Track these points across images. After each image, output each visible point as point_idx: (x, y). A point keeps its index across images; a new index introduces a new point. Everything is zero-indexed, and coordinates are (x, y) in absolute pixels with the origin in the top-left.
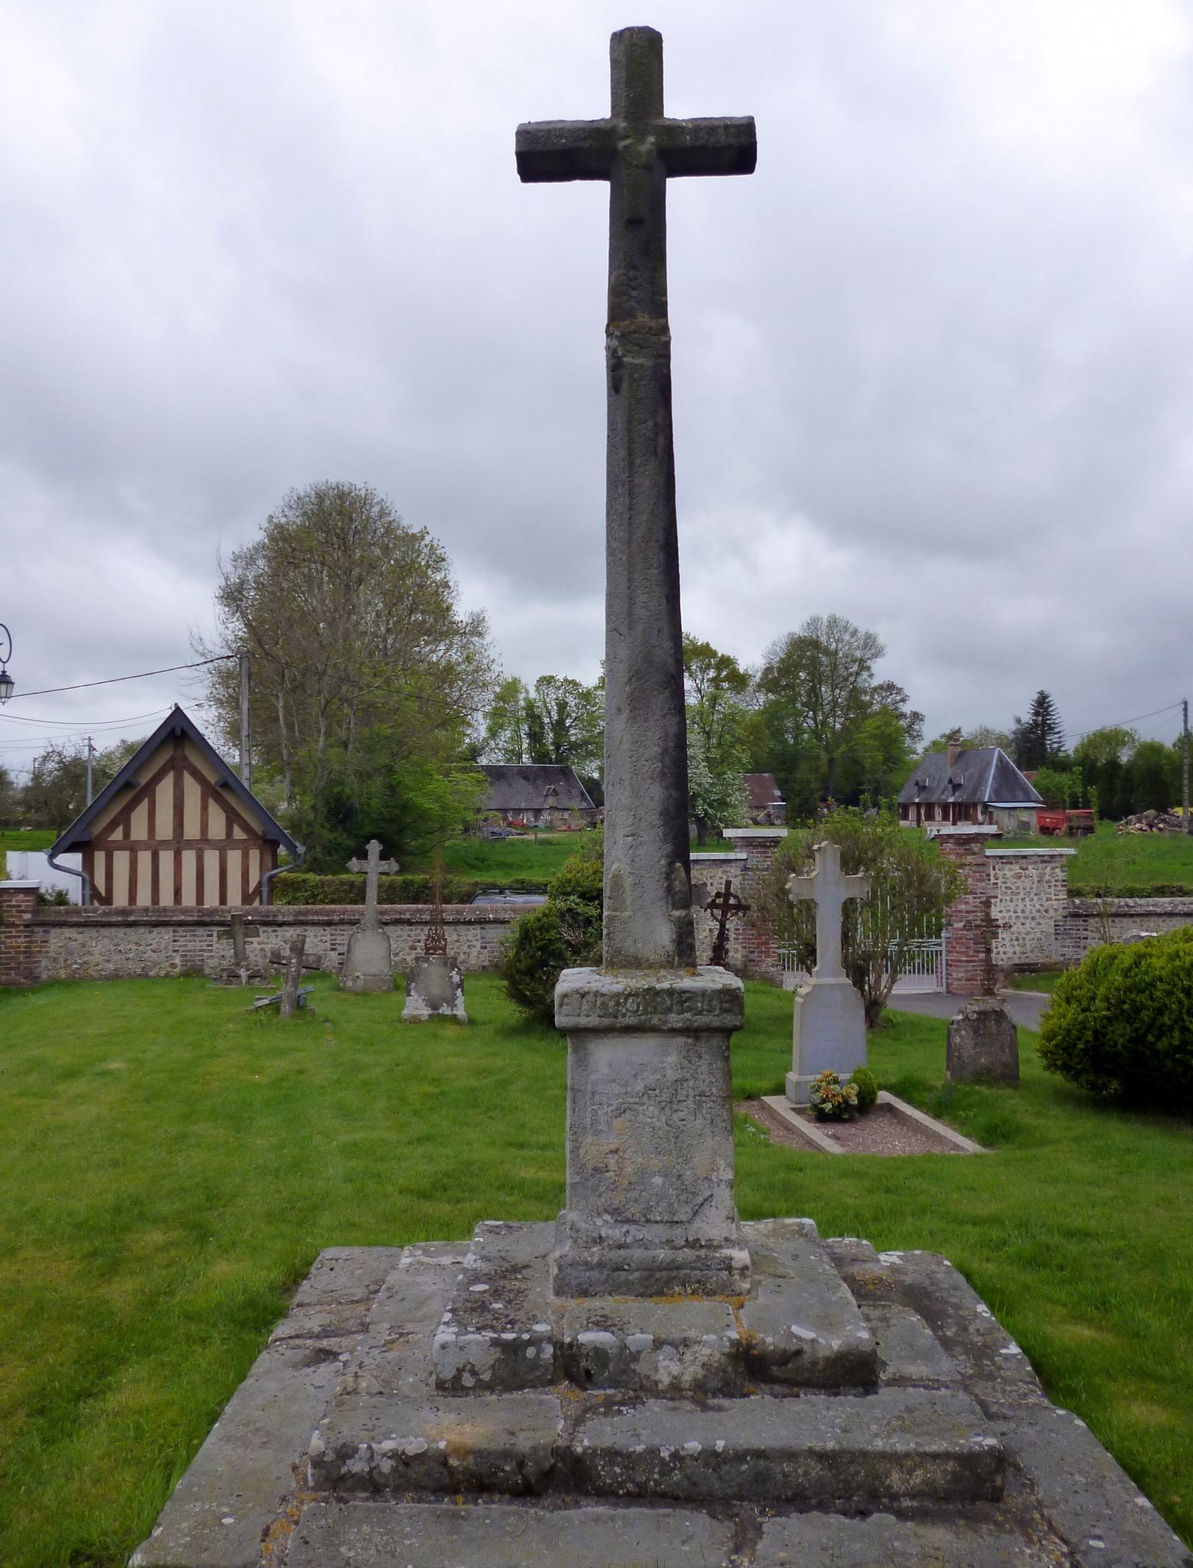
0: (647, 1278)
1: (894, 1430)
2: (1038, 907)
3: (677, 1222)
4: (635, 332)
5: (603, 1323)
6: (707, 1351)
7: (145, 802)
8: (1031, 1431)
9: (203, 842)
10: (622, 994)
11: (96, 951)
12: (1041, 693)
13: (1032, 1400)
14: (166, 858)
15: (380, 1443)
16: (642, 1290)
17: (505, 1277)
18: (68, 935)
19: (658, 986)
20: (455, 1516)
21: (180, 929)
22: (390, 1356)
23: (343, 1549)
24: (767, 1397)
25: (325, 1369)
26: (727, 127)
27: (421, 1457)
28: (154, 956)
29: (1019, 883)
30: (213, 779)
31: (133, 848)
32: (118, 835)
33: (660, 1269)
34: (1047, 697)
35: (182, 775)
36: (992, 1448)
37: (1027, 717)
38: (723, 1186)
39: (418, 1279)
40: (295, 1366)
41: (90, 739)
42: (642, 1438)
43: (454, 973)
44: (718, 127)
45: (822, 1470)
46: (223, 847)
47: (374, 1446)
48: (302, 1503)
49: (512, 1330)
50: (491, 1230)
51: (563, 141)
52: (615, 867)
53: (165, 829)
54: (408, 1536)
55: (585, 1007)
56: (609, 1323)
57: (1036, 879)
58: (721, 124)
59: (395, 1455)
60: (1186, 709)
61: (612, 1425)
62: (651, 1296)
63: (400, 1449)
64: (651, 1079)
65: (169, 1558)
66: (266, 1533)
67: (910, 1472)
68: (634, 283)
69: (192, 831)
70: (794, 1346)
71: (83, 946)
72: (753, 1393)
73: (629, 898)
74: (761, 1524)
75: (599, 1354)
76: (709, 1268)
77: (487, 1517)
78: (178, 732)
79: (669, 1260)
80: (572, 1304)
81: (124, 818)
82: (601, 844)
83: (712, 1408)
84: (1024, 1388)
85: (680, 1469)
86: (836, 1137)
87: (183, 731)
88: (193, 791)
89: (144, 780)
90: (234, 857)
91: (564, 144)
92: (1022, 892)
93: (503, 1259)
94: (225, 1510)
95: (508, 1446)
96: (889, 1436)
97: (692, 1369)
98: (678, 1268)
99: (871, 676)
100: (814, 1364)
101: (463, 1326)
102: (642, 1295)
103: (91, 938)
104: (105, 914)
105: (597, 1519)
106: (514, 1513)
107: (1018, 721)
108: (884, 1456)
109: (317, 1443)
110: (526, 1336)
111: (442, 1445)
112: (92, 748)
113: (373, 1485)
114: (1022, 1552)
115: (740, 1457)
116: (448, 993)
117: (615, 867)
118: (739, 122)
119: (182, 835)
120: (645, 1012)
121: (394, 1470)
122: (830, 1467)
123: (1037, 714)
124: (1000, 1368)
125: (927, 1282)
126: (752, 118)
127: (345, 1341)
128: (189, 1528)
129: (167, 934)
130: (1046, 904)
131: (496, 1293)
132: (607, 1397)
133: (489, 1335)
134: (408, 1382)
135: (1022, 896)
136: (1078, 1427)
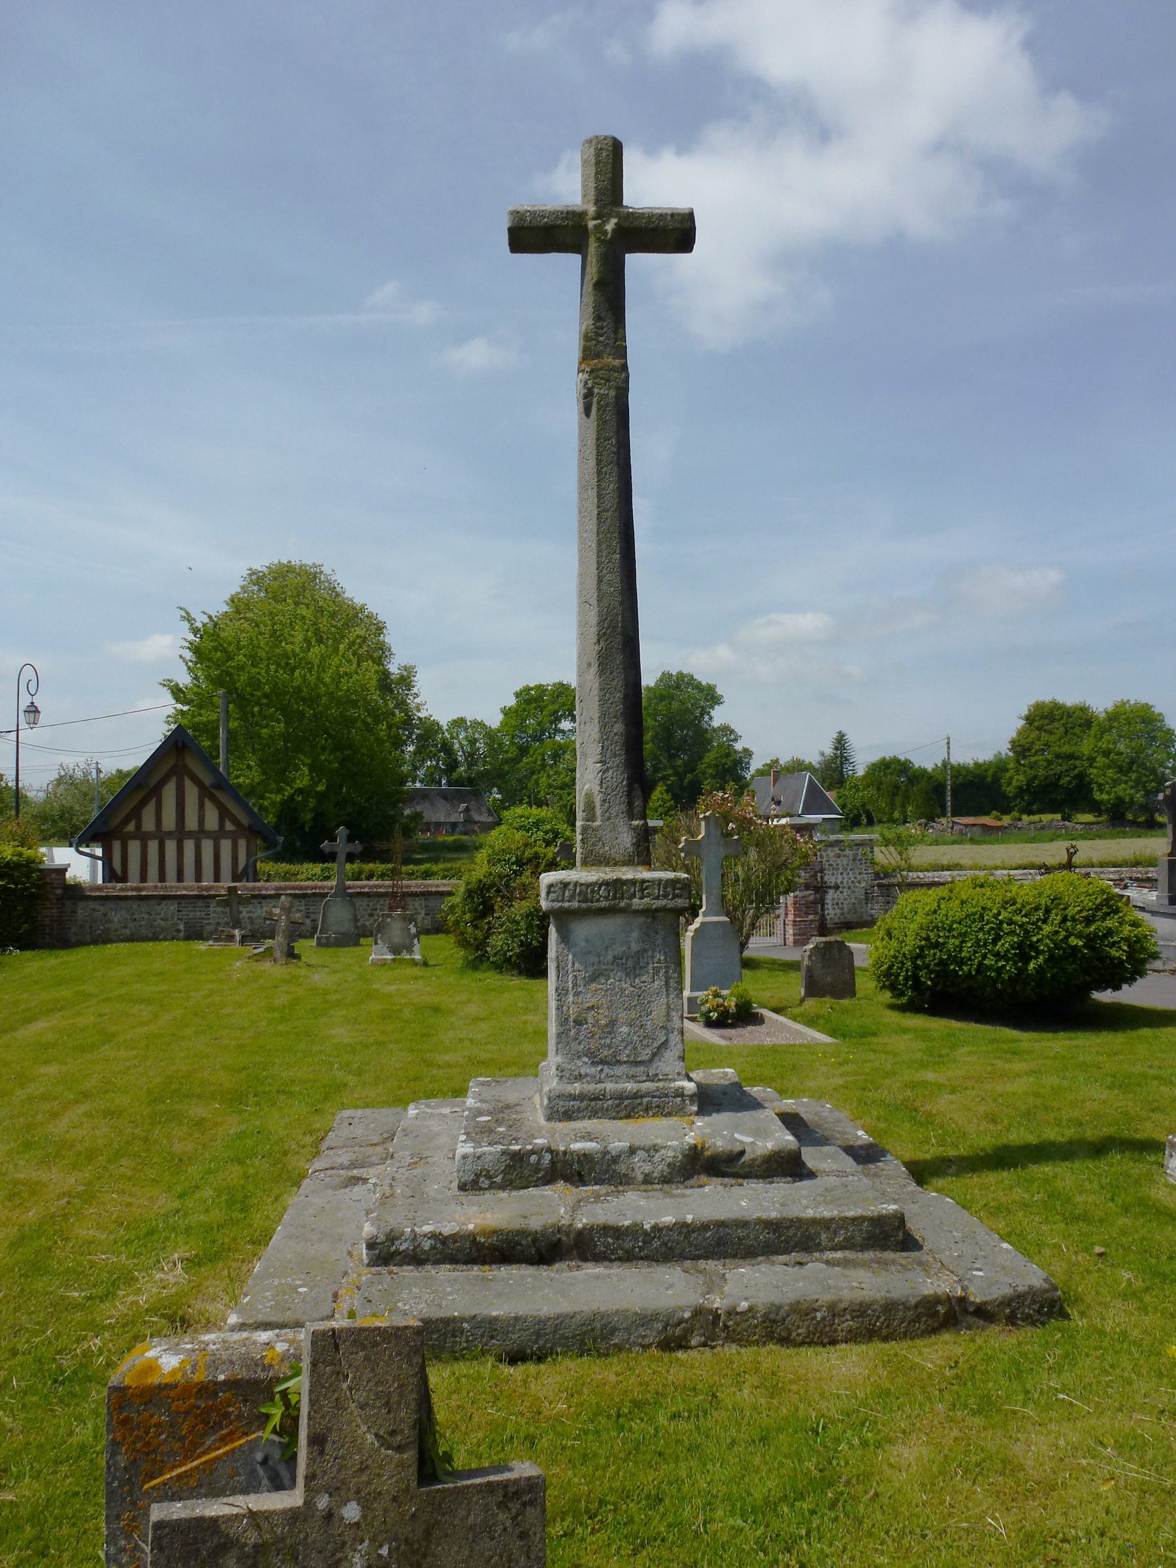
0: (618, 1105)
1: (820, 1203)
2: (852, 879)
3: (640, 1062)
4: (601, 369)
5: (588, 1137)
6: (671, 1153)
7: (153, 803)
8: (915, 1207)
9: (200, 834)
10: (596, 883)
11: (116, 919)
12: (840, 732)
13: (910, 1189)
14: (171, 846)
15: (421, 1227)
16: (613, 1114)
17: (503, 1112)
18: (92, 907)
19: (624, 877)
20: (484, 1279)
21: (182, 901)
22: (415, 1172)
23: (399, 1304)
24: (720, 1188)
25: (358, 1190)
26: (672, 215)
27: (454, 1237)
28: (163, 923)
29: (839, 861)
30: (207, 780)
31: (144, 838)
32: (131, 827)
33: (627, 1098)
34: (844, 736)
35: (183, 780)
36: (896, 1211)
37: (829, 751)
38: (676, 1033)
39: (426, 1123)
40: (335, 1188)
41: (97, 763)
42: (628, 1216)
43: (412, 926)
44: (666, 214)
45: (768, 1233)
46: (216, 837)
47: (416, 1229)
48: (360, 1275)
49: (517, 1143)
50: (483, 1084)
51: (546, 220)
52: (586, 787)
53: (169, 822)
54: (449, 1294)
55: (567, 894)
56: (593, 1136)
57: (851, 858)
58: (670, 212)
59: (433, 1236)
60: (948, 743)
61: (603, 1209)
62: (621, 1119)
63: (438, 1231)
64: (619, 949)
65: (260, 1316)
66: (335, 1296)
67: (835, 1233)
68: (600, 332)
69: (191, 823)
70: (737, 1148)
71: (105, 915)
72: (708, 1184)
73: (598, 812)
74: (724, 1275)
75: (586, 1157)
76: (666, 1096)
77: (510, 1279)
78: (180, 745)
79: (634, 1091)
80: (560, 1126)
81: (136, 814)
82: (574, 770)
83: (677, 1196)
84: (903, 1182)
85: (659, 1238)
86: (722, 1037)
87: (183, 743)
88: (192, 793)
89: (153, 782)
90: (226, 845)
91: (547, 223)
92: (841, 868)
93: (498, 1101)
94: (298, 1282)
95: (523, 1226)
96: (816, 1207)
97: (660, 1168)
98: (642, 1097)
99: (711, 718)
100: (754, 1160)
101: (478, 1144)
102: (614, 1118)
103: (111, 909)
104: (121, 889)
105: (598, 1277)
106: (531, 1276)
107: (822, 754)
108: (814, 1221)
109: (368, 1229)
110: (529, 1147)
111: (471, 1227)
112: (99, 771)
113: (416, 1259)
114: (925, 1282)
115: (705, 1227)
116: (407, 941)
117: (586, 787)
118: (682, 212)
119: (183, 826)
120: (614, 898)
121: (433, 1247)
122: (775, 1232)
123: (836, 748)
124: (883, 1170)
125: (816, 1119)
126: (690, 217)
127: (372, 1171)
128: (272, 1295)
129: (173, 907)
130: (859, 877)
131: (499, 1122)
132: (594, 1191)
133: (500, 1147)
134: (433, 1189)
135: (841, 871)
136: (948, 1202)
